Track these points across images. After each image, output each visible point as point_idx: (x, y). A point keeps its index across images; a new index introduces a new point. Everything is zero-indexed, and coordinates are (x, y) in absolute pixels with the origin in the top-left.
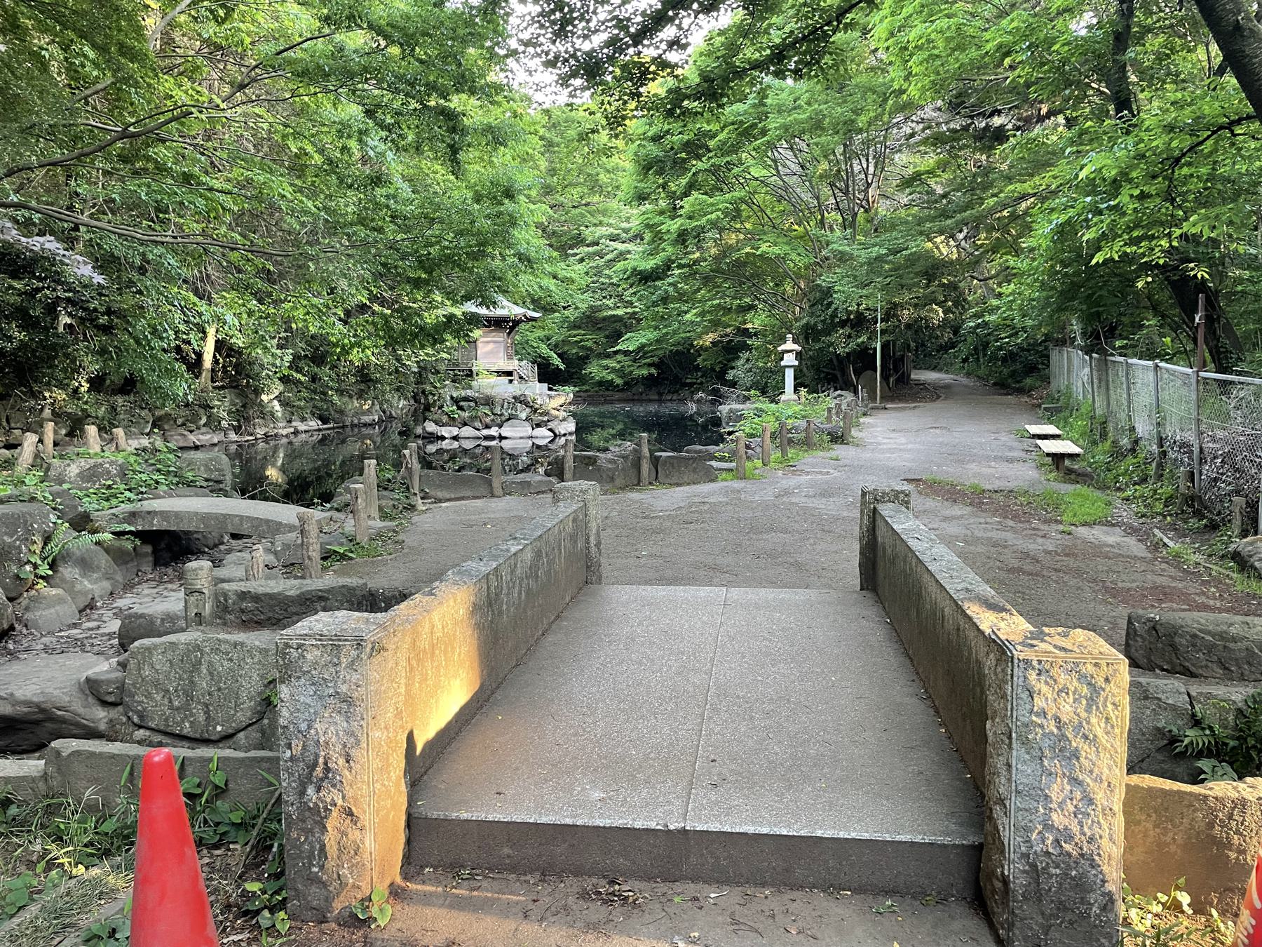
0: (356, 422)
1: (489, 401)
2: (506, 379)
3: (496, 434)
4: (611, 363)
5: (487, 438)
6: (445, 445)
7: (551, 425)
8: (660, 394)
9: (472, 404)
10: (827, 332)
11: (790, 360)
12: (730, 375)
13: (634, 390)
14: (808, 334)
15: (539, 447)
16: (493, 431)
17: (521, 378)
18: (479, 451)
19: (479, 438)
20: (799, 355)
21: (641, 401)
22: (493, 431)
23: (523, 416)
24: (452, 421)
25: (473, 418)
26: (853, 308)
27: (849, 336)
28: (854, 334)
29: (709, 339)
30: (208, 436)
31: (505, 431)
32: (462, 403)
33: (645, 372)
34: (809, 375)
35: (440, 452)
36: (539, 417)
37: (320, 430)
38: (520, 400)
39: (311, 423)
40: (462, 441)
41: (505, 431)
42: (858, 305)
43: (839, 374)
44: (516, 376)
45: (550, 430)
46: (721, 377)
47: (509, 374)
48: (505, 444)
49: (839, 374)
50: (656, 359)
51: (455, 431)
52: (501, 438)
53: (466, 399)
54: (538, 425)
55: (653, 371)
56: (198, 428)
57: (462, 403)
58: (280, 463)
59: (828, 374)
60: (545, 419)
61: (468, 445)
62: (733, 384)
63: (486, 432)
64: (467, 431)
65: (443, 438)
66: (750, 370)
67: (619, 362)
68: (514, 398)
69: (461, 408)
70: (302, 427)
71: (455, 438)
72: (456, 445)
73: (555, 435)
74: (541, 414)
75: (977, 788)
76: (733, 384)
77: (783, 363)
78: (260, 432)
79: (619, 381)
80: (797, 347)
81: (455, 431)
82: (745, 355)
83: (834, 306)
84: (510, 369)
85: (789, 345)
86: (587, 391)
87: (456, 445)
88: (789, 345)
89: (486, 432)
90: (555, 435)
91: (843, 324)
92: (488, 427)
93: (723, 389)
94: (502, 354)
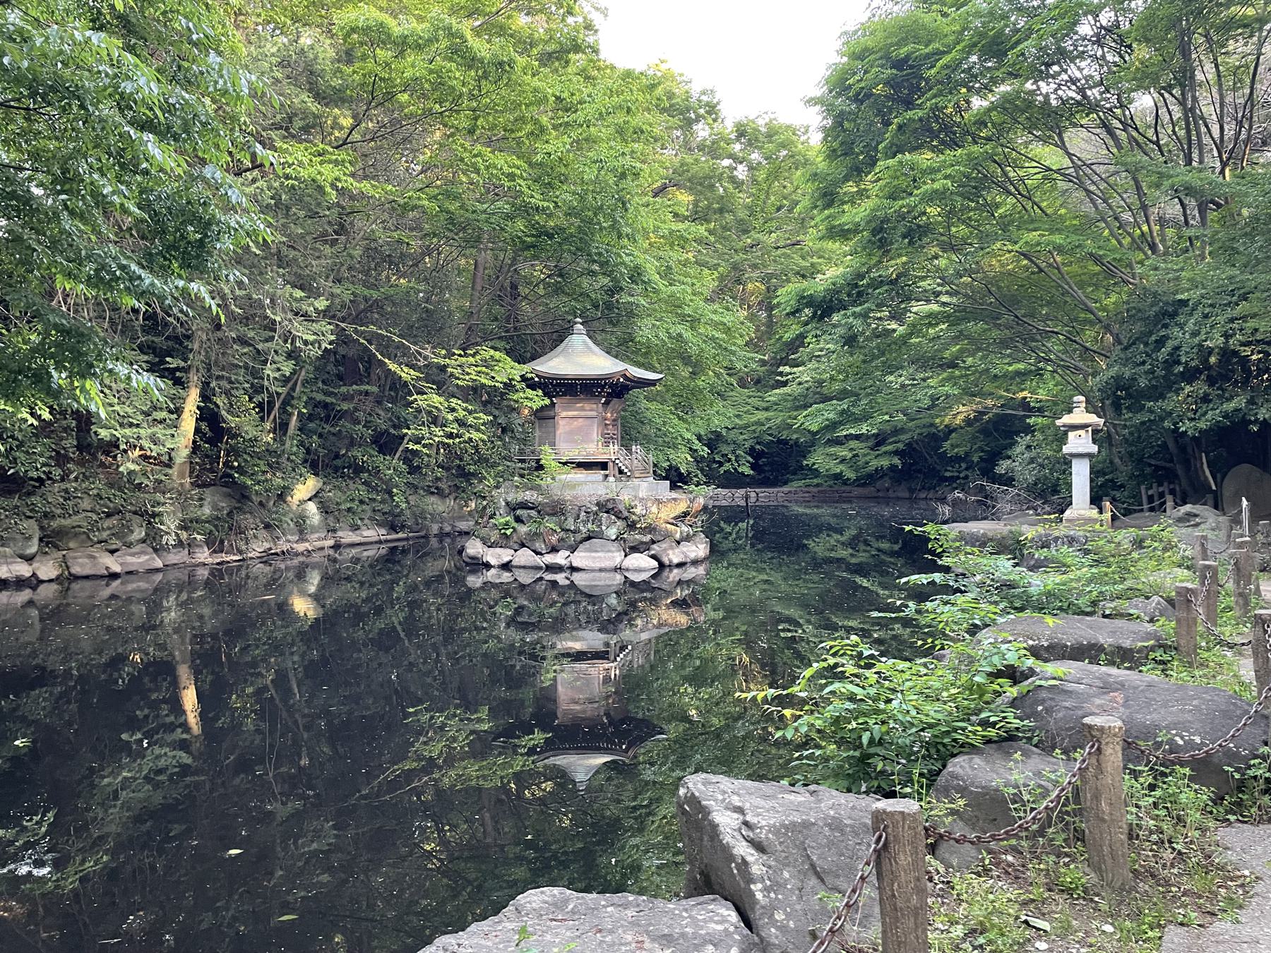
0: (448, 529)
1: (557, 510)
2: (598, 475)
3: (563, 562)
4: (844, 452)
5: (551, 568)
6: (491, 575)
7: (656, 549)
8: (911, 491)
9: (533, 513)
10: (1157, 392)
11: (1079, 443)
12: (1003, 467)
13: (878, 484)
14: (1116, 398)
15: (633, 584)
16: (560, 558)
17: (621, 472)
18: (541, 587)
19: (538, 568)
20: (1096, 435)
21: (887, 501)
22: (560, 558)
23: (612, 532)
24: (504, 541)
25: (536, 535)
26: (1216, 341)
27: (1206, 399)
28: (1214, 392)
29: (961, 412)
30: (144, 558)
31: (579, 559)
32: (519, 512)
33: (885, 462)
34: (1124, 471)
35: (487, 585)
36: (638, 534)
37: (387, 541)
38: (607, 507)
39: (366, 533)
40: (517, 572)
41: (579, 559)
42: (1227, 336)
43: (1180, 470)
44: (611, 470)
45: (653, 557)
46: (987, 469)
47: (603, 466)
48: (578, 578)
49: (1180, 470)
50: (901, 446)
51: (505, 555)
52: (574, 569)
53: (524, 505)
54: (634, 549)
55: (896, 461)
56: (129, 545)
57: (519, 512)
58: (312, 589)
59: (1157, 468)
60: (647, 538)
61: (526, 578)
62: (1008, 481)
63: (550, 559)
64: (524, 557)
65: (488, 566)
66: (1032, 461)
67: (851, 449)
68: (598, 504)
69: (518, 520)
70: (348, 537)
71: (506, 567)
72: (506, 577)
73: (662, 566)
74: (644, 531)
75: (1238, 569)
76: (1008, 481)
77: (1066, 449)
78: (258, 548)
79: (851, 475)
80: (1093, 419)
81: (505, 555)
82: (1023, 440)
83: (1170, 344)
84: (601, 458)
85: (1080, 415)
86: (818, 485)
87: (506, 577)
88: (1080, 415)
89: (550, 559)
90: (662, 566)
91: (1190, 375)
92: (554, 550)
93: (989, 486)
94: (595, 433)
